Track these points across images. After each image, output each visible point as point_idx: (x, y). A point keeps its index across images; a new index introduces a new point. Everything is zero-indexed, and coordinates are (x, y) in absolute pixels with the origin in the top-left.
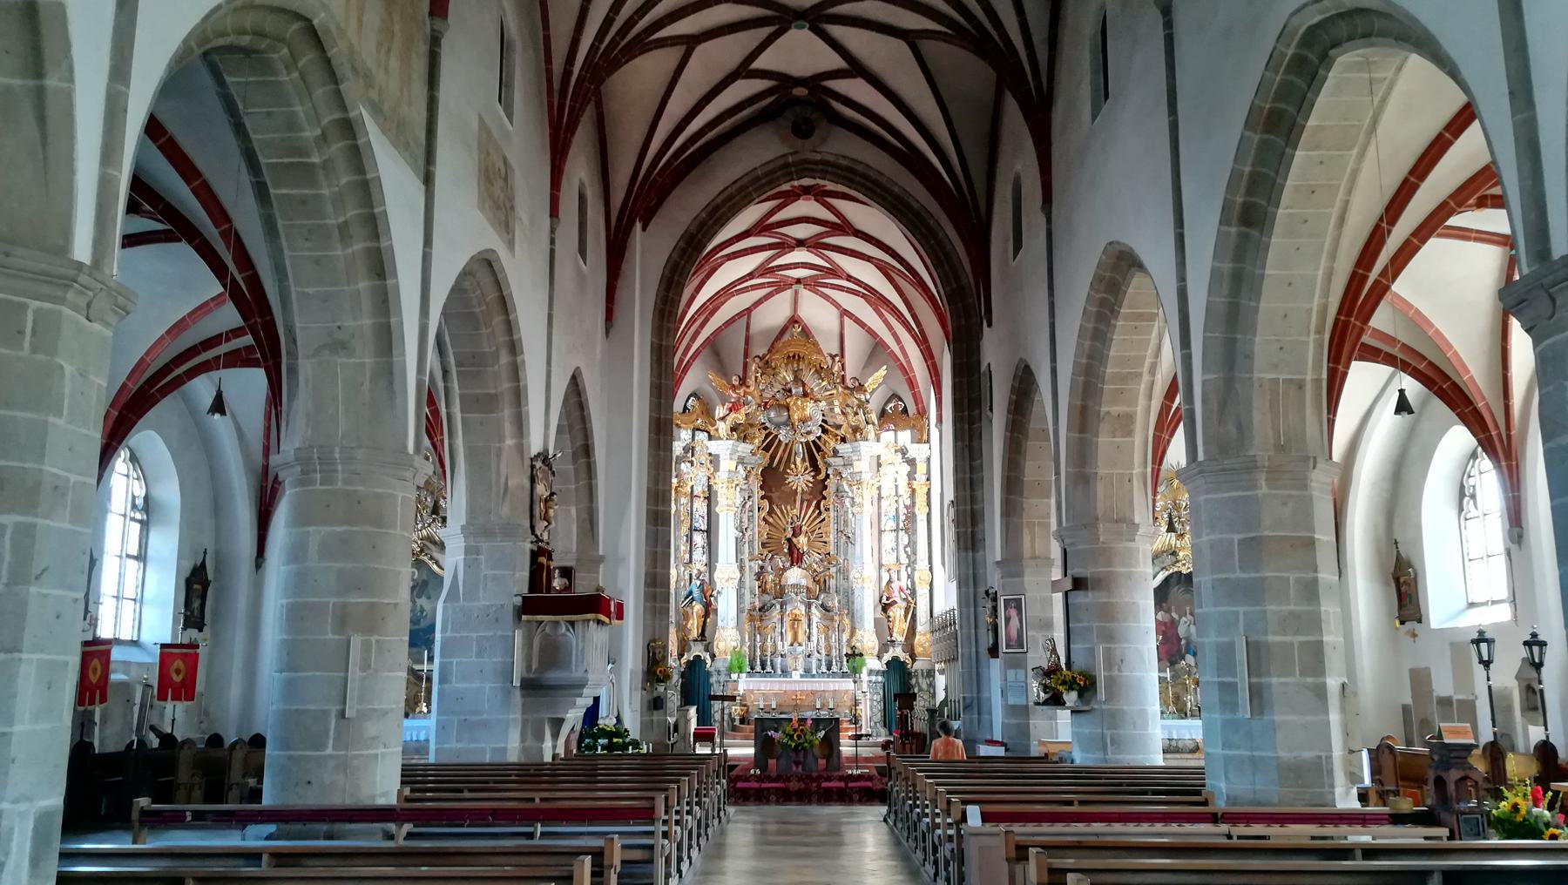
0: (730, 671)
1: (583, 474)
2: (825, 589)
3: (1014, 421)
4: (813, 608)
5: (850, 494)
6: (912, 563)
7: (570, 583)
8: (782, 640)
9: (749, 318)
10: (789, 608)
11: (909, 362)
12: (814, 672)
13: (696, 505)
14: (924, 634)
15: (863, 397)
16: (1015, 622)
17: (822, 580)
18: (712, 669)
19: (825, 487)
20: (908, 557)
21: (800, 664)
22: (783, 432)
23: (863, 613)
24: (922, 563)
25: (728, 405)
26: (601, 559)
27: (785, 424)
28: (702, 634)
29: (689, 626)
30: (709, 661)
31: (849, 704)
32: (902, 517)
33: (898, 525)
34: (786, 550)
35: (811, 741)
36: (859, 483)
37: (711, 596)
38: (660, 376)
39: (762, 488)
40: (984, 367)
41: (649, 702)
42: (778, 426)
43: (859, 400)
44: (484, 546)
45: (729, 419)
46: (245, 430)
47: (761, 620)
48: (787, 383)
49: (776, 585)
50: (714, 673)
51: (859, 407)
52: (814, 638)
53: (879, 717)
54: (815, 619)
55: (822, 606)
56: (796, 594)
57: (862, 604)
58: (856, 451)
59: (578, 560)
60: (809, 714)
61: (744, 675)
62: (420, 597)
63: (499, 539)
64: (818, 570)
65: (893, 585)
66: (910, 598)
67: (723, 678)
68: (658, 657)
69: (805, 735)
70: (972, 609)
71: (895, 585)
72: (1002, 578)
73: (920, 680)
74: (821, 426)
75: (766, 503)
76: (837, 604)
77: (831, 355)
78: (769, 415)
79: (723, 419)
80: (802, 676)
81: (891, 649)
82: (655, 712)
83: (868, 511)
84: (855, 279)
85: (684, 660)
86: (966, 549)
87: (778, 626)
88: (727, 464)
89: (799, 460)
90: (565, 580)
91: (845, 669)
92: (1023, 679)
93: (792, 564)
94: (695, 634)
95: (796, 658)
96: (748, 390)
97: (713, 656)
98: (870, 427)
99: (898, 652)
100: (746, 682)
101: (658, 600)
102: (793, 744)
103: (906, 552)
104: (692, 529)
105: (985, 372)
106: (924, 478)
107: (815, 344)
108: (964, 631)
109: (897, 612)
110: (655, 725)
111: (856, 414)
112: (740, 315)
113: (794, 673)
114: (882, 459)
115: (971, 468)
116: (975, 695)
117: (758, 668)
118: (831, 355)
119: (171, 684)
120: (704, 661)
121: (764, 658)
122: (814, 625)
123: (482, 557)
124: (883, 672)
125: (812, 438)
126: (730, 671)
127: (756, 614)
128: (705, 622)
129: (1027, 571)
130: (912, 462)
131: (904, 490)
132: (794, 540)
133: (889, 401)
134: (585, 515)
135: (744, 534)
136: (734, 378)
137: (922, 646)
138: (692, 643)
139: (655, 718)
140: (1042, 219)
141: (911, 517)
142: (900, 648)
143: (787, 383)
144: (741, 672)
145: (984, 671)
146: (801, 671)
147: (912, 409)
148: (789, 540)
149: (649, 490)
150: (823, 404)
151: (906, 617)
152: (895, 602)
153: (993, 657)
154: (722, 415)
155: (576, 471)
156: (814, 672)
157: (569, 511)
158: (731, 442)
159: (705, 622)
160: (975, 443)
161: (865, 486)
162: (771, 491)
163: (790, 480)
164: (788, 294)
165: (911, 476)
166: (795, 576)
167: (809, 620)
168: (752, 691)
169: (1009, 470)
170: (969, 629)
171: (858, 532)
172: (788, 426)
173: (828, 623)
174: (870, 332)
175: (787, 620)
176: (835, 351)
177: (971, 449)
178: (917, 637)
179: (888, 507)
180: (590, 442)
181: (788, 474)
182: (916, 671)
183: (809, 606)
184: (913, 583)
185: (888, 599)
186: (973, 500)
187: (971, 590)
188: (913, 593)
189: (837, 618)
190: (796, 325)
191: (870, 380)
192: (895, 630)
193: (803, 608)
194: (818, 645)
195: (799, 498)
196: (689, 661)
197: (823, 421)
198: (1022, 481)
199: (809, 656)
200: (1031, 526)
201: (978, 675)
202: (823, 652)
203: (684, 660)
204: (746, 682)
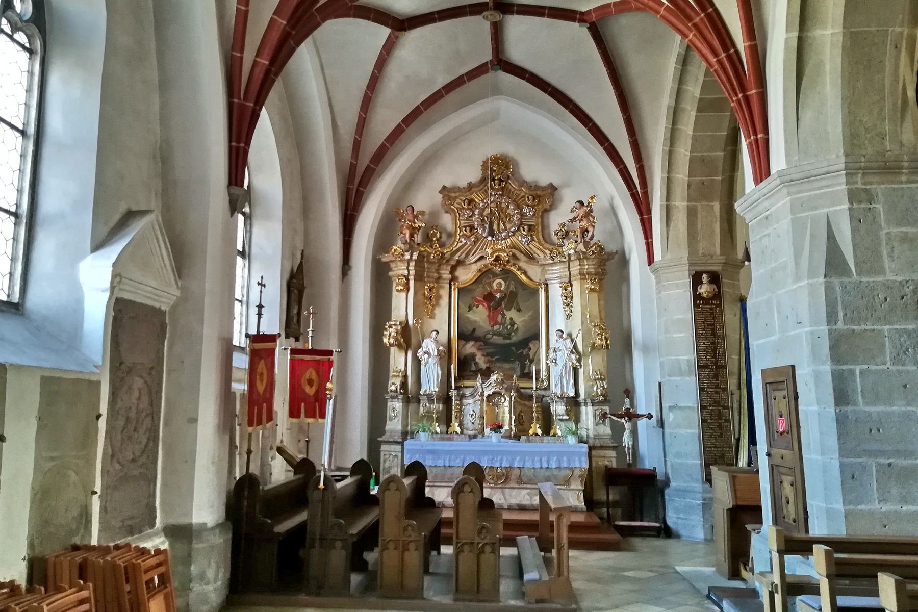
7: (719, 288)
44: (879, 188)
46: (339, 123)
62: (509, 309)
63: (904, 178)
117: (536, 428)
119: (305, 398)
123: (879, 207)
157: (712, 207)
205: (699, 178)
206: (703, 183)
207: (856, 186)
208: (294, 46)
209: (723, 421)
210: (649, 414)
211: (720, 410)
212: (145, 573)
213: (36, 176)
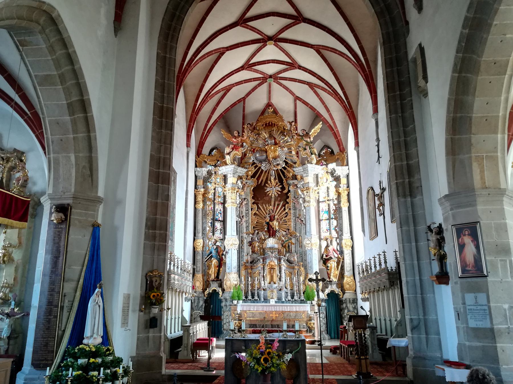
0: (232, 299)
1: (81, 126)
2: (289, 251)
3: (463, 60)
4: (282, 261)
5: (303, 196)
6: (340, 236)
8: (264, 280)
9: (244, 103)
10: (268, 261)
11: (334, 123)
12: (284, 300)
13: (217, 207)
14: (350, 277)
15: (309, 140)
16: (470, 249)
17: (287, 246)
18: (222, 298)
19: (288, 197)
20: (337, 233)
21: (275, 294)
22: (264, 165)
23: (312, 264)
24: (346, 235)
25: (232, 146)
26: (98, 201)
27: (265, 161)
28: (217, 277)
29: (210, 272)
30: (221, 293)
31: (305, 320)
32: (332, 212)
33: (329, 216)
34: (266, 229)
35: (278, 365)
36: (308, 189)
37: (223, 255)
38: (163, 78)
39: (253, 198)
40: (412, 51)
41: (147, 321)
42: (261, 162)
43: (307, 141)
45: (232, 154)
47: (252, 269)
48: (266, 139)
49: (260, 249)
50: (224, 300)
51: (307, 145)
52: (283, 279)
53: (324, 328)
54: (283, 268)
55: (287, 260)
56: (272, 253)
57: (311, 259)
58: (306, 171)
59: (75, 198)
60: (276, 336)
61: (241, 301)
64: (285, 240)
65: (329, 248)
66: (340, 256)
67: (228, 303)
68: (156, 284)
69: (272, 358)
70: (414, 244)
71: (331, 248)
72: (451, 209)
73: (348, 305)
74: (285, 161)
75: (255, 206)
76: (296, 259)
77: (289, 122)
78: (256, 155)
79: (229, 154)
80: (276, 302)
81: (330, 286)
82: (151, 330)
83: (313, 205)
84: (303, 67)
85: (206, 292)
86: (405, 196)
87: (262, 272)
88: (231, 180)
89: (272, 178)
90: (61, 215)
91: (302, 298)
92: (485, 302)
93: (269, 237)
94: (213, 277)
95: (272, 291)
96: (243, 139)
97: (223, 290)
98: (313, 156)
99: (334, 288)
100: (242, 305)
101: (157, 239)
102: (260, 369)
103: (336, 230)
104: (214, 220)
105: (415, 60)
106: (346, 186)
107: (281, 117)
108: (408, 262)
109: (332, 264)
110: (151, 342)
111: (305, 149)
112: (239, 101)
113: (271, 300)
114: (320, 176)
115: (405, 133)
116: (421, 317)
117: (250, 297)
118: (289, 122)
120: (218, 293)
121: (253, 291)
122: (283, 271)
124: (326, 300)
125: (279, 168)
126: (232, 299)
127: (249, 265)
128: (219, 270)
129: (480, 200)
130: (337, 179)
131: (333, 195)
132: (270, 223)
133: (322, 150)
134: (84, 163)
135: (241, 219)
136: (235, 132)
137: (348, 284)
138: (211, 282)
139: (151, 335)
140: (355, 153)
141: (338, 210)
142: (335, 285)
143: (266, 139)
144: (239, 299)
145: (429, 296)
146: (276, 299)
147: (336, 150)
148: (268, 224)
149: (152, 156)
150: (286, 149)
151: (338, 268)
152: (331, 258)
153: (440, 283)
154: (228, 152)
155: (74, 122)
156: (284, 300)
157: (69, 157)
158: (233, 166)
159: (219, 270)
160: (407, 115)
161: (311, 190)
162: (258, 200)
163: (268, 190)
164: (265, 86)
165: (337, 187)
166: (271, 242)
167: (280, 268)
168: (245, 311)
169: (455, 112)
170: (412, 260)
171: (307, 217)
172: (266, 161)
173: (291, 270)
174: (312, 108)
175: (267, 268)
176: (292, 119)
177: (403, 118)
178: (345, 279)
179: (323, 206)
180: (85, 98)
181: (267, 187)
182: (346, 299)
183: (279, 260)
184: (341, 247)
185: (326, 256)
186: (408, 157)
187: (412, 228)
188: (342, 252)
189: (296, 267)
190: (270, 108)
191: (313, 131)
192: (332, 274)
193: (276, 262)
194: (285, 283)
195: (273, 200)
196: (209, 294)
197: (286, 158)
198: (471, 118)
199: (280, 290)
200: (480, 159)
201: (423, 300)
202: (289, 287)
203: (206, 292)
204: (242, 305)
205: (57, 136)
206: (62, 140)
207: (500, 259)
208: (170, 23)
209: (52, 317)
210: (323, 278)
211: (51, 308)
212: (451, 138)
213: (263, 14)
